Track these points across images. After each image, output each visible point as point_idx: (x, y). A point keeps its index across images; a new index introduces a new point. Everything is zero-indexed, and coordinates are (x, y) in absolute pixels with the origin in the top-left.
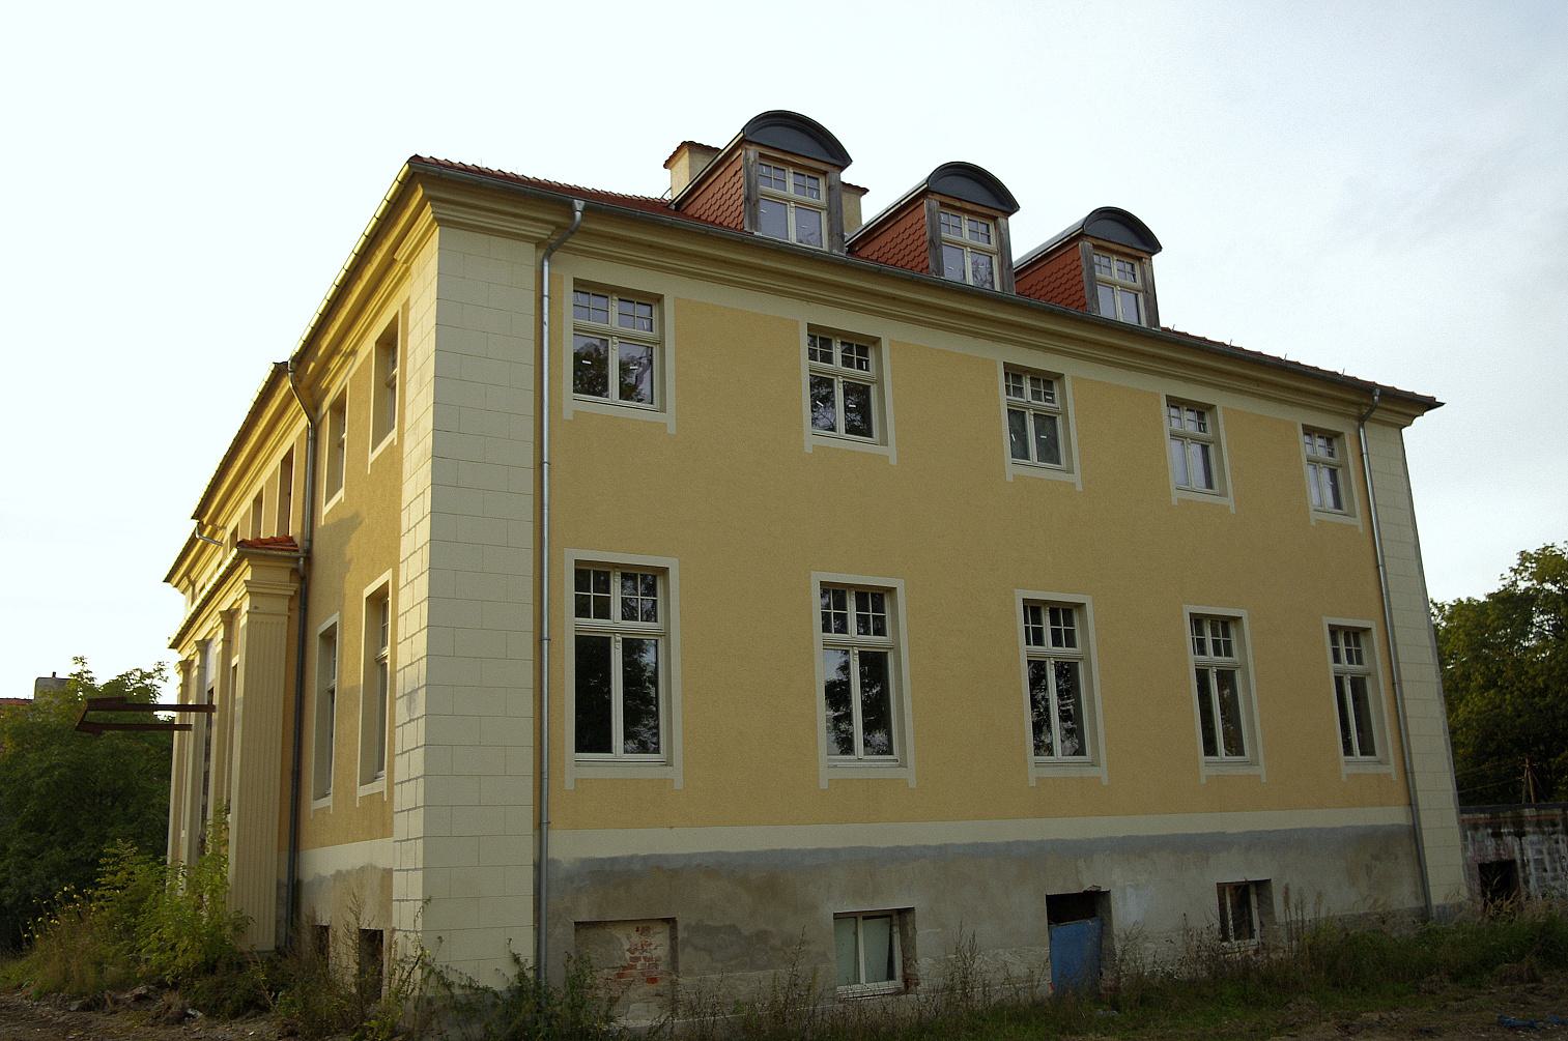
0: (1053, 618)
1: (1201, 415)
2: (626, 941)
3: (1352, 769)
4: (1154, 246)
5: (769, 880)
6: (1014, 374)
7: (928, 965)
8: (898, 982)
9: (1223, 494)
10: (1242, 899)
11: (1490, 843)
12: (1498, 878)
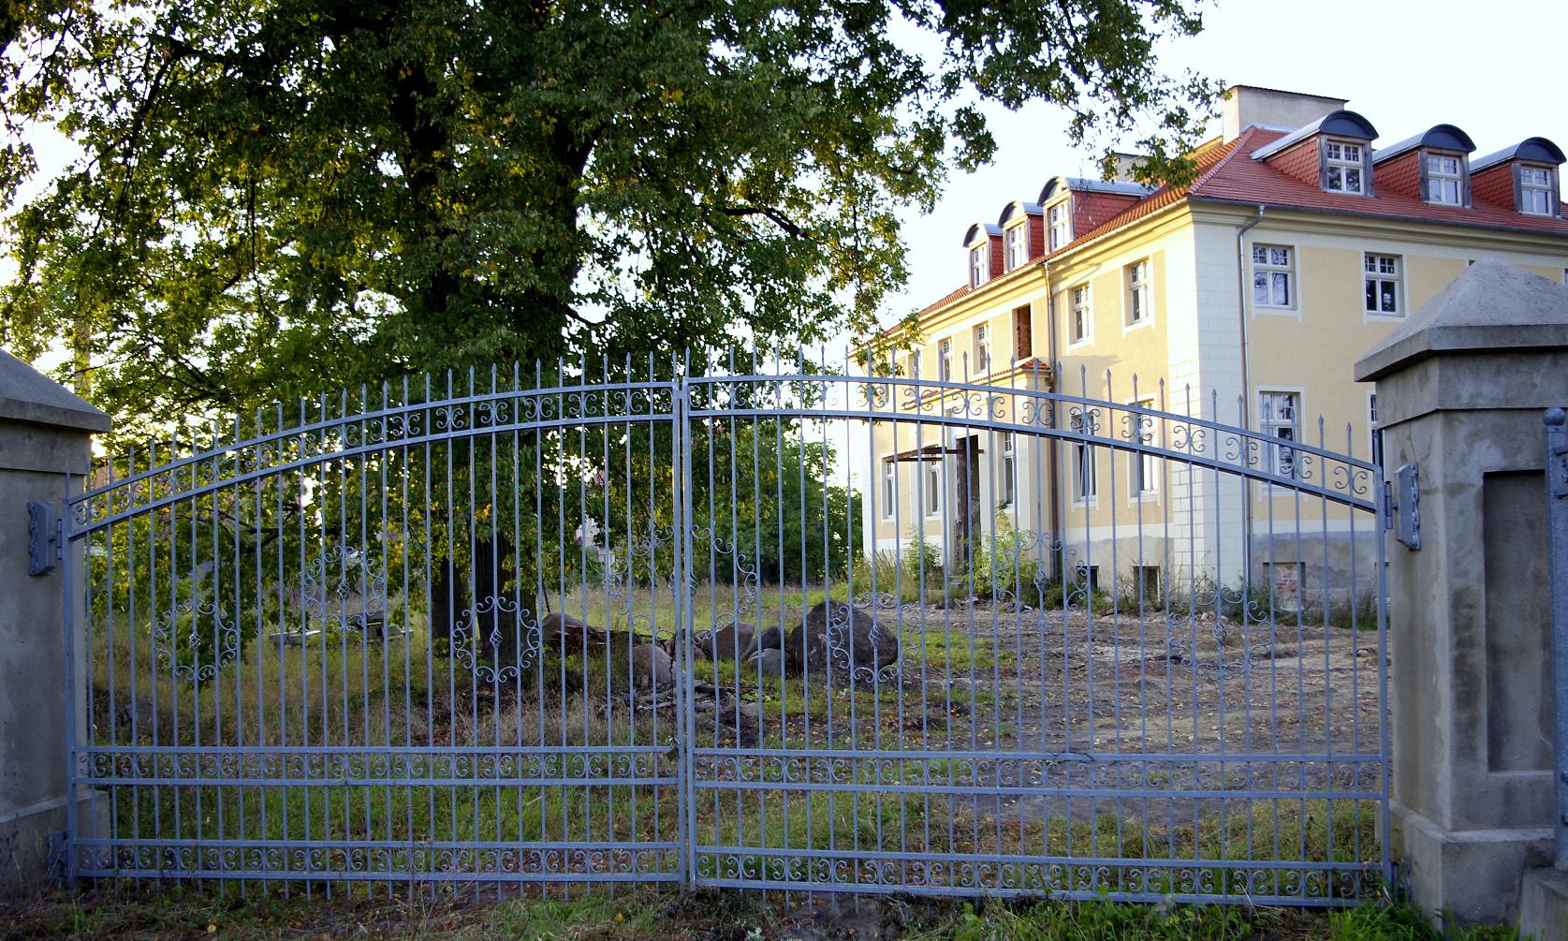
2: (1283, 571)
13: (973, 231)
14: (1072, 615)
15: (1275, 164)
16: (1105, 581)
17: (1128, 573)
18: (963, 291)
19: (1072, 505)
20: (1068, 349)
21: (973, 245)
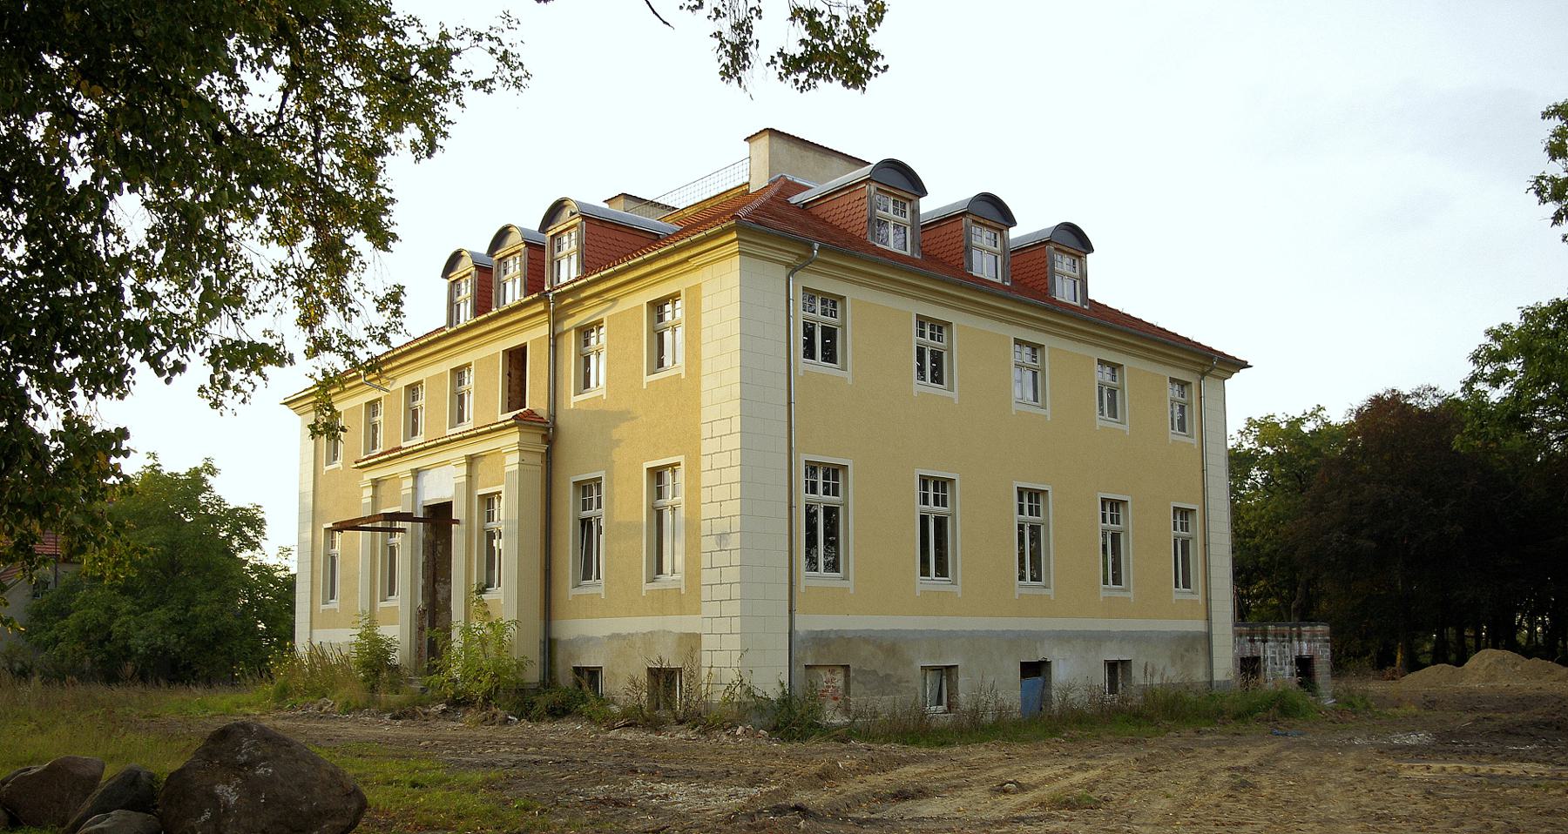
0: (1032, 498)
1: (1034, 350)
2: (825, 675)
3: (1180, 597)
4: (1090, 249)
5: (891, 646)
6: (921, 321)
7: (964, 697)
8: (945, 707)
9: (1043, 407)
10: (1115, 669)
11: (1248, 645)
12: (1250, 666)
13: (455, 258)
14: (567, 729)
15: (815, 212)
16: (607, 686)
17: (643, 677)
18: (442, 329)
19: (568, 588)
20: (572, 400)
21: (454, 275)
